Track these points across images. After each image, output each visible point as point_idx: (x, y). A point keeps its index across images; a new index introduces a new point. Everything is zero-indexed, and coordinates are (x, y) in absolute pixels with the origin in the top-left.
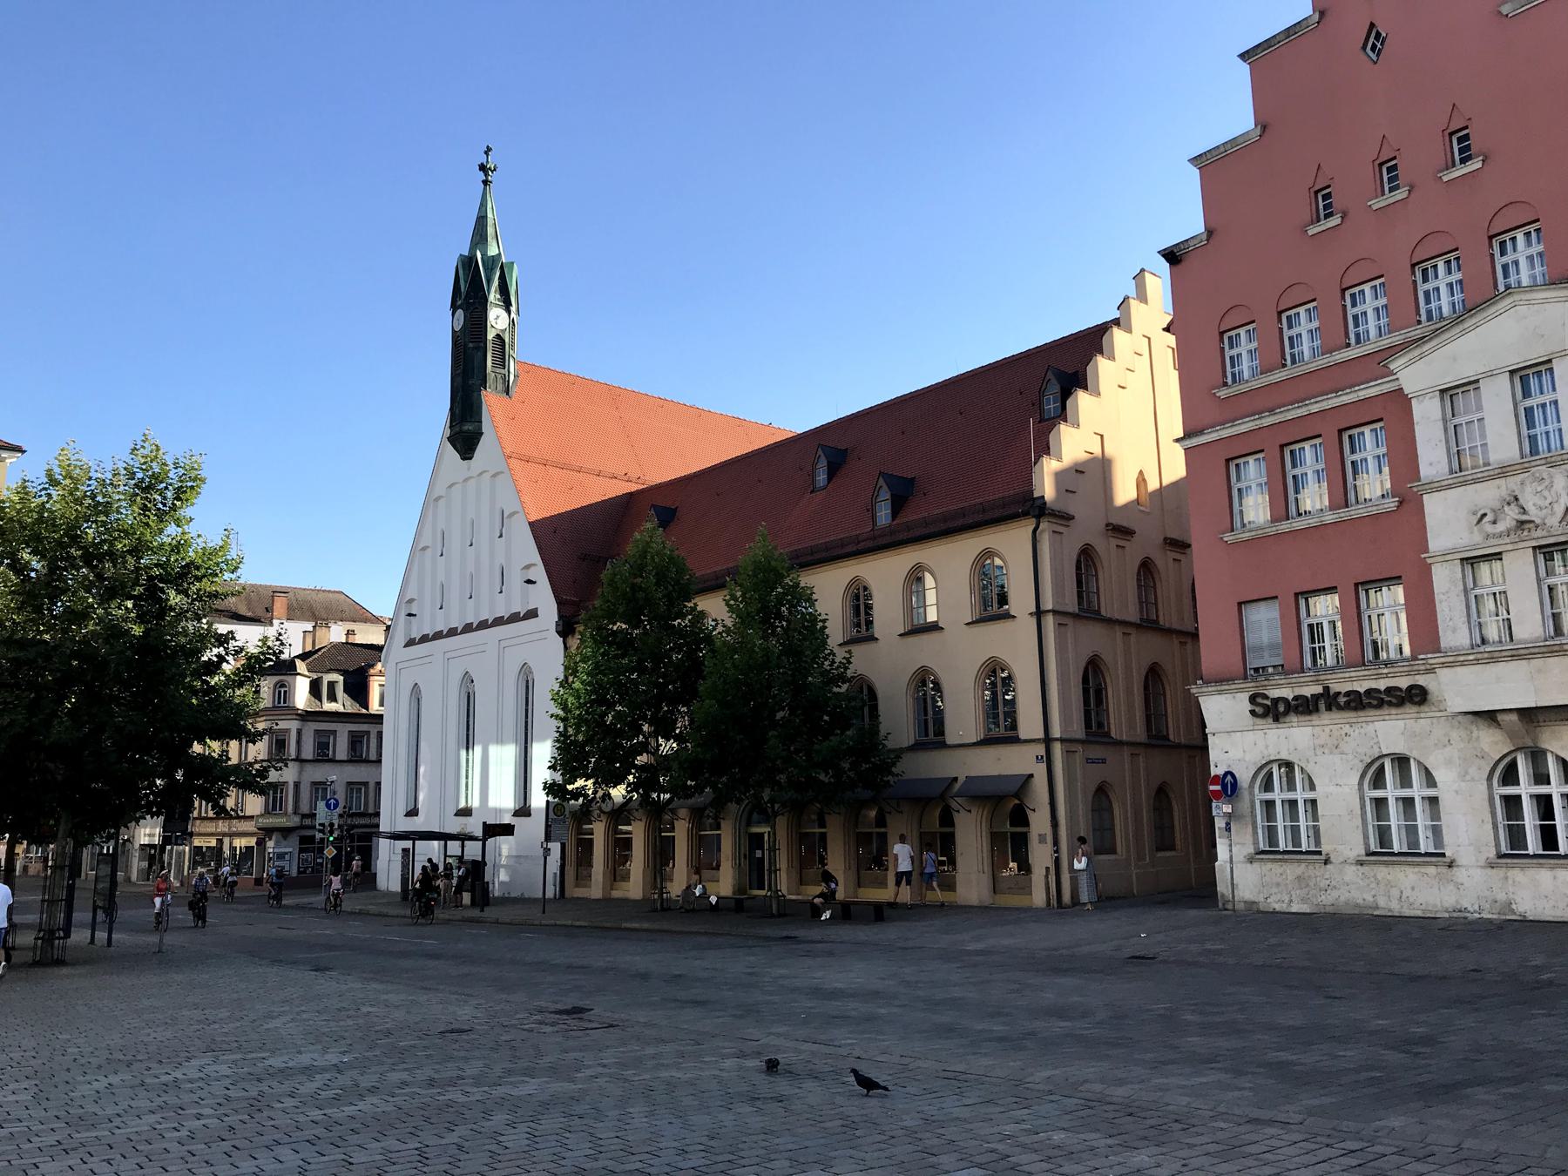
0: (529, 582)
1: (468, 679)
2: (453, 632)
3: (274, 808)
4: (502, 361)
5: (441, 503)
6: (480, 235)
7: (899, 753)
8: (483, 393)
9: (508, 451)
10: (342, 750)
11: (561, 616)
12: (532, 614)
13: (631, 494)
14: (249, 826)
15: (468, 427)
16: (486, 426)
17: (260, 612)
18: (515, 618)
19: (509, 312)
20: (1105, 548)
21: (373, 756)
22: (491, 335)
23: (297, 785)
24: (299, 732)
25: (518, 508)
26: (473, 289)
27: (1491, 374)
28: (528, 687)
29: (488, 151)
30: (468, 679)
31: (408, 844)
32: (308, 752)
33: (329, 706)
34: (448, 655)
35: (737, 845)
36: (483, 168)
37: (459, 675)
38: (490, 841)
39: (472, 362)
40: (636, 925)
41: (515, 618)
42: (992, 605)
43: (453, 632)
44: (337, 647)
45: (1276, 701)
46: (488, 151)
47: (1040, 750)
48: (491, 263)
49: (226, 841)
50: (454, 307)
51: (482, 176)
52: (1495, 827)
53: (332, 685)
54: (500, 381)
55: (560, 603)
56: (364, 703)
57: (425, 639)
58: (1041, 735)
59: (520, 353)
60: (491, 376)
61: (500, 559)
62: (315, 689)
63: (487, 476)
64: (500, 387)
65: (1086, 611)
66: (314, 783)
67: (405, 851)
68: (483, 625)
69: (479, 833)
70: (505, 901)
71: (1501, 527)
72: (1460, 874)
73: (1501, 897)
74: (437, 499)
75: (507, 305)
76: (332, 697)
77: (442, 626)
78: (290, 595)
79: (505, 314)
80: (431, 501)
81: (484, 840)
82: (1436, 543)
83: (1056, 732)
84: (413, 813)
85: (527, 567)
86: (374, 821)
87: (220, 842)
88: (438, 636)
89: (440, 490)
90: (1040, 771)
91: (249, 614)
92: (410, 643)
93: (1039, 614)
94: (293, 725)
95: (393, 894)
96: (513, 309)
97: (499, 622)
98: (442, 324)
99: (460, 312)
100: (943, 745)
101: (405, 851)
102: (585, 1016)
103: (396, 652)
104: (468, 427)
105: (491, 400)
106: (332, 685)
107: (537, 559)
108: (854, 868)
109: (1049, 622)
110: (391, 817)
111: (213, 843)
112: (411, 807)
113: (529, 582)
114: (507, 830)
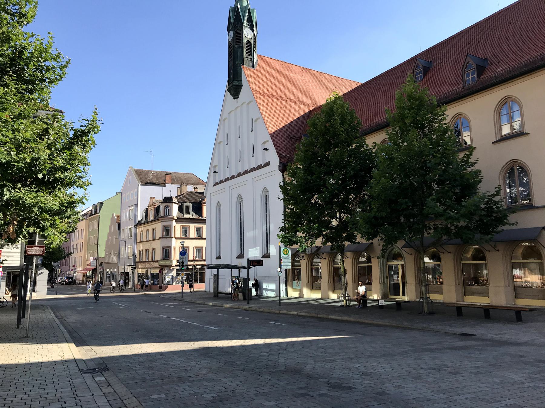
1: (240, 198)
2: (233, 177)
3: (166, 257)
4: (250, 52)
5: (226, 121)
8: (242, 66)
9: (254, 91)
10: (192, 233)
11: (280, 163)
12: (268, 164)
13: (310, 111)
14: (156, 265)
15: (236, 83)
16: (244, 82)
17: (162, 181)
18: (259, 167)
19: (253, 31)
22: (245, 41)
25: (259, 116)
26: (237, 21)
28: (267, 198)
30: (240, 198)
31: (215, 271)
33: (186, 216)
34: (231, 188)
35: (382, 272)
37: (236, 196)
38: (252, 270)
39: (238, 54)
40: (339, 318)
41: (259, 167)
43: (233, 177)
44: (190, 193)
48: (244, 9)
49: (149, 270)
50: (229, 31)
53: (187, 207)
54: (250, 62)
55: (280, 157)
56: (200, 214)
57: (221, 182)
59: (259, 50)
60: (245, 60)
61: (252, 142)
62: (181, 209)
63: (245, 105)
64: (250, 64)
68: (246, 172)
69: (246, 265)
74: (224, 120)
75: (252, 27)
76: (188, 212)
77: (228, 176)
79: (251, 32)
80: (222, 121)
81: (248, 268)
84: (219, 258)
85: (264, 143)
87: (147, 271)
88: (227, 180)
89: (225, 116)
91: (157, 182)
92: (216, 184)
95: (209, 293)
96: (255, 29)
97: (253, 170)
98: (223, 39)
99: (231, 32)
100: (531, 207)
101: (215, 275)
104: (236, 83)
105: (246, 69)
106: (187, 207)
108: (461, 285)
111: (145, 272)
112: (265, 253)
113: (265, 149)
114: (259, 263)
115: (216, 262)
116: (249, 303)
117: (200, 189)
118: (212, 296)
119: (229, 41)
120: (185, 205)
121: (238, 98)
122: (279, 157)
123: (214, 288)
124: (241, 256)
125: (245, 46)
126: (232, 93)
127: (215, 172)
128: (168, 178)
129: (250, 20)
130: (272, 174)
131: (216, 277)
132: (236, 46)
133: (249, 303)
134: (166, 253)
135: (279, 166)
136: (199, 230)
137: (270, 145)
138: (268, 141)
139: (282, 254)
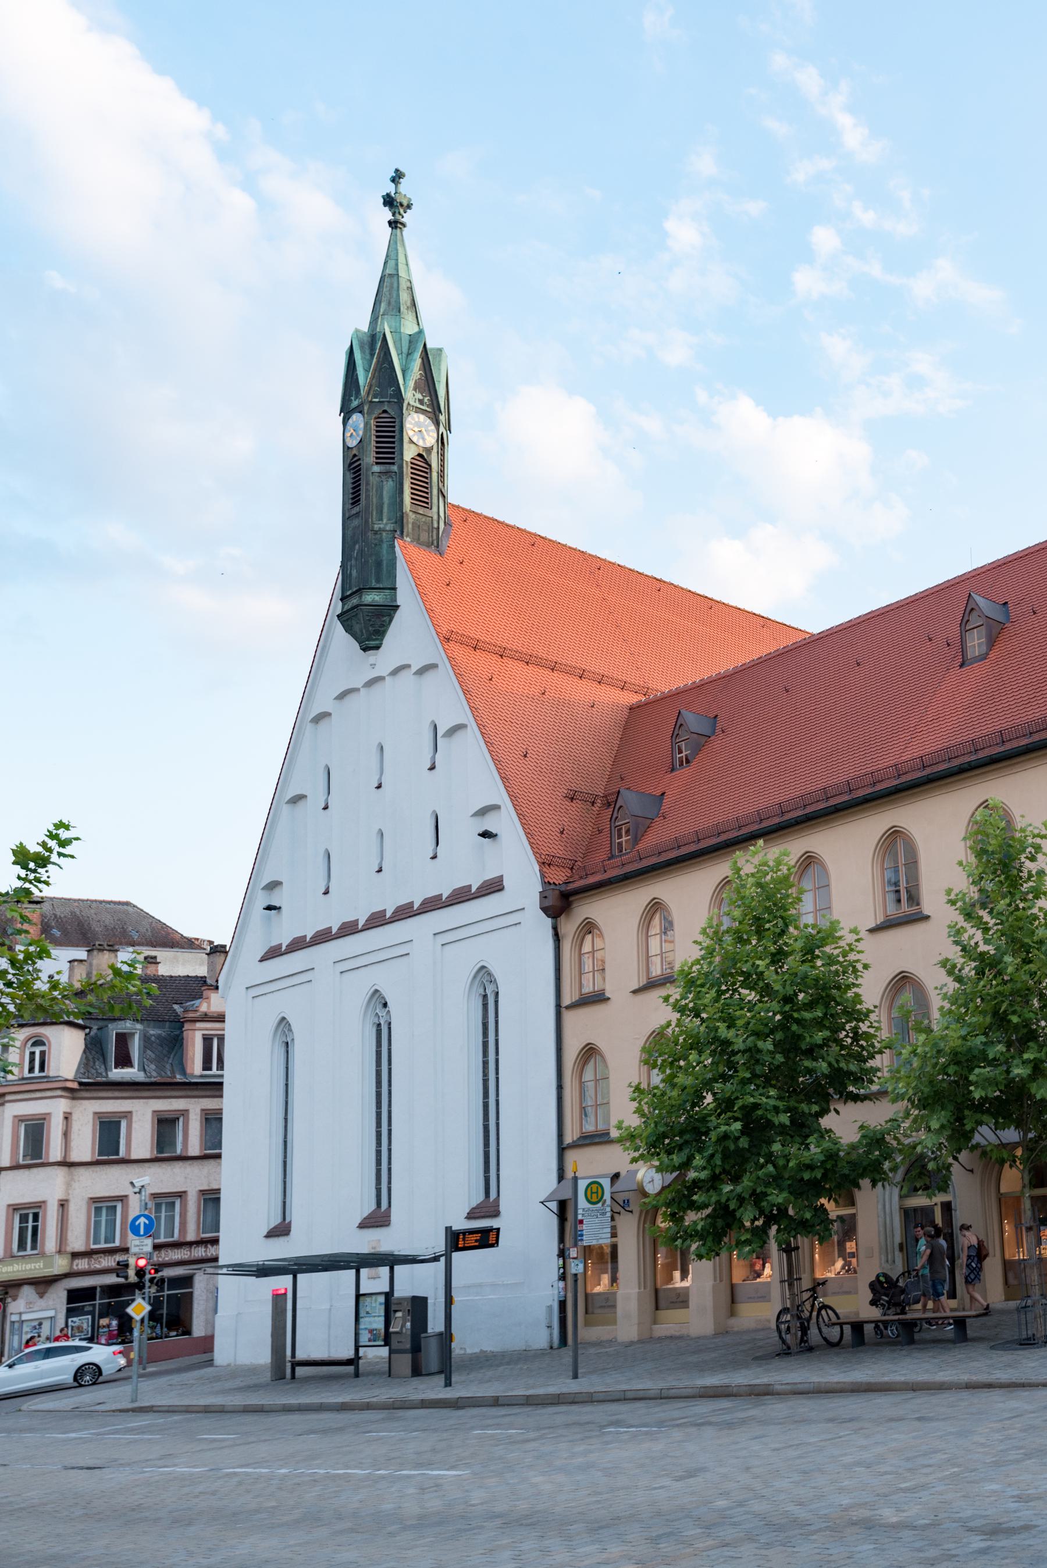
0: (486, 834)
2: (349, 929)
3: (22, 1246)
6: (391, 293)
7: (734, 1211)
10: (140, 1138)
11: (546, 883)
12: (494, 887)
15: (371, 597)
18: (462, 896)
22: (409, 453)
23: (63, 1205)
24: (67, 1117)
29: (397, 177)
31: (283, 1282)
32: (84, 1147)
33: (118, 1074)
36: (389, 201)
41: (462, 896)
43: (349, 929)
46: (397, 177)
50: (347, 411)
51: (387, 214)
53: (123, 1040)
57: (298, 945)
63: (407, 676)
66: (94, 1200)
67: (278, 1299)
68: (405, 912)
69: (439, 1245)
70: (484, 1361)
78: (46, 907)
79: (433, 427)
80: (312, 719)
84: (281, 1231)
85: (483, 812)
86: (211, 1251)
88: (323, 937)
89: (323, 702)
92: (273, 953)
94: (56, 1107)
95: (253, 1370)
96: (442, 418)
97: (433, 904)
98: (323, 437)
99: (357, 419)
102: (1034, 1532)
103: (242, 973)
107: (501, 797)
110: (241, 1238)
112: (276, 1220)
113: (486, 834)
116: (448, 1383)
117: (174, 965)
118: (267, 1376)
119: (346, 449)
120: (114, 1030)
121: (377, 648)
123: (278, 1348)
124: (378, 1219)
125: (407, 471)
126: (357, 628)
127: (269, 908)
129: (428, 383)
132: (376, 468)
133: (448, 1383)
134: (22, 1231)
135: (543, 896)
136: (166, 1126)
137: (507, 823)
138: (496, 808)
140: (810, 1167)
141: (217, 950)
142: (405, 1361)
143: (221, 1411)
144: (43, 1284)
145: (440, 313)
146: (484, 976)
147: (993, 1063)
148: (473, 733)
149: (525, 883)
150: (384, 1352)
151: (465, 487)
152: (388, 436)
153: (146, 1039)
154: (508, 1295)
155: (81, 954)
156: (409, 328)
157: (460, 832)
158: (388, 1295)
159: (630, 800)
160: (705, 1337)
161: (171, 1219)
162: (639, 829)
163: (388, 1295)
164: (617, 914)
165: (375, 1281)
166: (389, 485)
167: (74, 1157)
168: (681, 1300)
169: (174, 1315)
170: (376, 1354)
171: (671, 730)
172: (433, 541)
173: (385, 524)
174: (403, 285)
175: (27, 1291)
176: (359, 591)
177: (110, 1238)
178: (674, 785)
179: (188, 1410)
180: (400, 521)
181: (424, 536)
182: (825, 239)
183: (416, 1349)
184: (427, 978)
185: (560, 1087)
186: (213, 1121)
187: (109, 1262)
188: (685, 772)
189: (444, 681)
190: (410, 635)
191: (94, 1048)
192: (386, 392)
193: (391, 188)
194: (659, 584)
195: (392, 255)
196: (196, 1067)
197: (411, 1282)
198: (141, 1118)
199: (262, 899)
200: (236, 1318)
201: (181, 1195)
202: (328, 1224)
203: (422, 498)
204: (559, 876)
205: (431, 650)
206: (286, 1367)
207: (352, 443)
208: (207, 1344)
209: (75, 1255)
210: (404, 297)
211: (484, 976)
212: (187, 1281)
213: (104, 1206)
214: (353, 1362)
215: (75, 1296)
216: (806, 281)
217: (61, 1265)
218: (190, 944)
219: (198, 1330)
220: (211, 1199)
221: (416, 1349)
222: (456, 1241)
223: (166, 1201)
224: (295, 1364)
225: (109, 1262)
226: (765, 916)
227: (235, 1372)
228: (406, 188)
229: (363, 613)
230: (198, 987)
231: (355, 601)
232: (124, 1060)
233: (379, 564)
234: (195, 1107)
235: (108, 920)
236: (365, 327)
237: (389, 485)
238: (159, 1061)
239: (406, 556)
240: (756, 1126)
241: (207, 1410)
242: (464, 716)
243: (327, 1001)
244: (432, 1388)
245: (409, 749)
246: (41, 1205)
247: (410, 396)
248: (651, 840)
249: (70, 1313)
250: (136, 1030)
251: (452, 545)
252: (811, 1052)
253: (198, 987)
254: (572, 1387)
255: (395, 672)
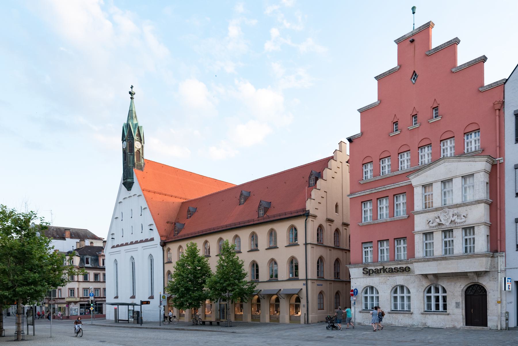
0: (151, 229)
2: (127, 244)
3: (71, 295)
6: (131, 115)
10: (91, 278)
12: (152, 239)
15: (129, 180)
18: (147, 240)
20: (325, 225)
21: (102, 280)
22: (135, 150)
23: (78, 289)
27: (436, 182)
29: (132, 87)
31: (116, 306)
33: (86, 265)
36: (130, 93)
41: (147, 240)
42: (293, 243)
43: (127, 244)
45: (370, 270)
46: (132, 87)
47: (305, 282)
52: (424, 304)
53: (87, 259)
57: (118, 246)
58: (305, 278)
63: (136, 196)
65: (320, 243)
67: (115, 309)
68: (137, 242)
69: (139, 303)
71: (434, 224)
72: (414, 316)
73: (424, 321)
82: (417, 229)
83: (309, 277)
84: (117, 297)
85: (150, 225)
88: (122, 245)
89: (121, 200)
90: (304, 288)
93: (306, 244)
95: (112, 321)
96: (142, 142)
97: (141, 241)
99: (125, 142)
107: (153, 223)
109: (309, 247)
110: (110, 298)
113: (151, 229)
114: (148, 303)
115: (130, 301)
117: (97, 244)
120: (85, 257)
122: (161, 236)
124: (133, 297)
125: (135, 154)
128: (67, 234)
129: (139, 135)
130: (156, 246)
131: (116, 311)
135: (161, 243)
136: (96, 276)
137: (154, 227)
139: (162, 299)
140: (196, 297)
141: (105, 242)
142: (136, 321)
143: (105, 326)
144: (76, 302)
145: (141, 120)
146: (151, 255)
147: (221, 284)
148: (148, 210)
149: (158, 240)
150: (133, 319)
151: (148, 155)
152: (131, 146)
153: (91, 259)
154: (153, 311)
155: (78, 240)
156: (135, 122)
157: (146, 228)
158: (133, 310)
159: (178, 225)
160: (85, 318)
161: (98, 293)
162: (179, 231)
163: (133, 310)
164: (174, 247)
165: (131, 308)
166: (132, 157)
167: (80, 280)
168: (184, 315)
169: (99, 309)
170: (132, 320)
171: (189, 209)
172: (141, 168)
173: (131, 165)
174: (134, 112)
175: (73, 304)
176: (126, 179)
177: (87, 295)
178: (187, 222)
179: (100, 325)
180: (134, 164)
181: (139, 168)
182: (275, 32)
183: (138, 319)
184: (141, 254)
185: (164, 277)
186: (104, 275)
187: (86, 300)
188: (190, 219)
189: (142, 198)
190: (136, 188)
191: (82, 260)
192: (130, 136)
193: (130, 90)
194: (191, 174)
195: (131, 106)
196: (101, 265)
197: (137, 308)
198: (91, 275)
199: (111, 237)
200: (109, 311)
201: (100, 289)
202: (125, 298)
203: (139, 160)
204: (164, 239)
205: (140, 192)
206: (117, 320)
207: (124, 148)
208: (105, 316)
209: (81, 298)
210: (134, 115)
211: (151, 255)
212: (101, 304)
213: (86, 290)
214: (128, 320)
215: (81, 305)
216: (269, 46)
217: (78, 299)
218: (100, 239)
219: (104, 313)
220: (104, 289)
221: (138, 319)
222: (142, 303)
223: (96, 289)
224: (119, 320)
225: (86, 300)
226: (193, 253)
227: (109, 321)
228: (134, 90)
229: (128, 184)
230: (101, 249)
231: (125, 181)
232: (88, 263)
233: (130, 173)
234: (101, 272)
235: (83, 233)
236: (126, 122)
237: (132, 157)
238: (94, 263)
239: (135, 171)
240: (187, 289)
241: (103, 326)
242: (146, 206)
243: (123, 257)
244: (139, 326)
245: (137, 212)
246: (74, 288)
247: (135, 138)
248: (181, 233)
249: (81, 308)
250: (90, 258)
251: (145, 169)
252: (199, 278)
253: (101, 249)
254: (159, 327)
255: (134, 195)
